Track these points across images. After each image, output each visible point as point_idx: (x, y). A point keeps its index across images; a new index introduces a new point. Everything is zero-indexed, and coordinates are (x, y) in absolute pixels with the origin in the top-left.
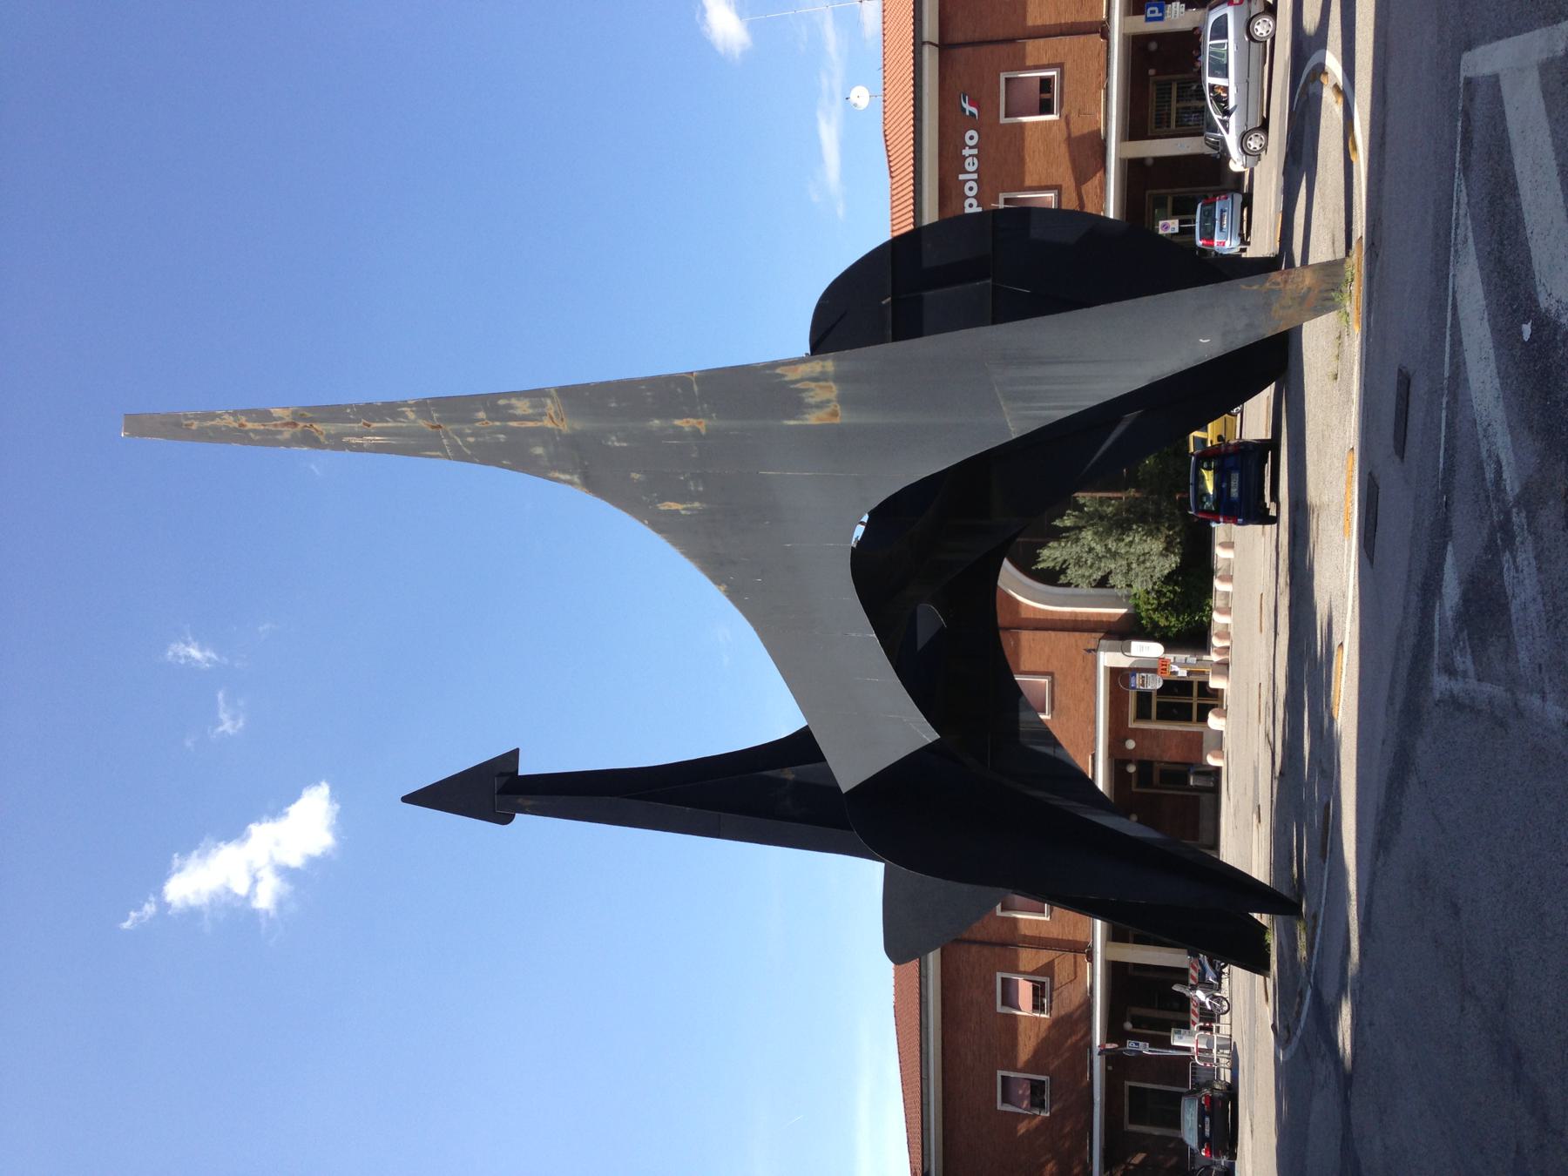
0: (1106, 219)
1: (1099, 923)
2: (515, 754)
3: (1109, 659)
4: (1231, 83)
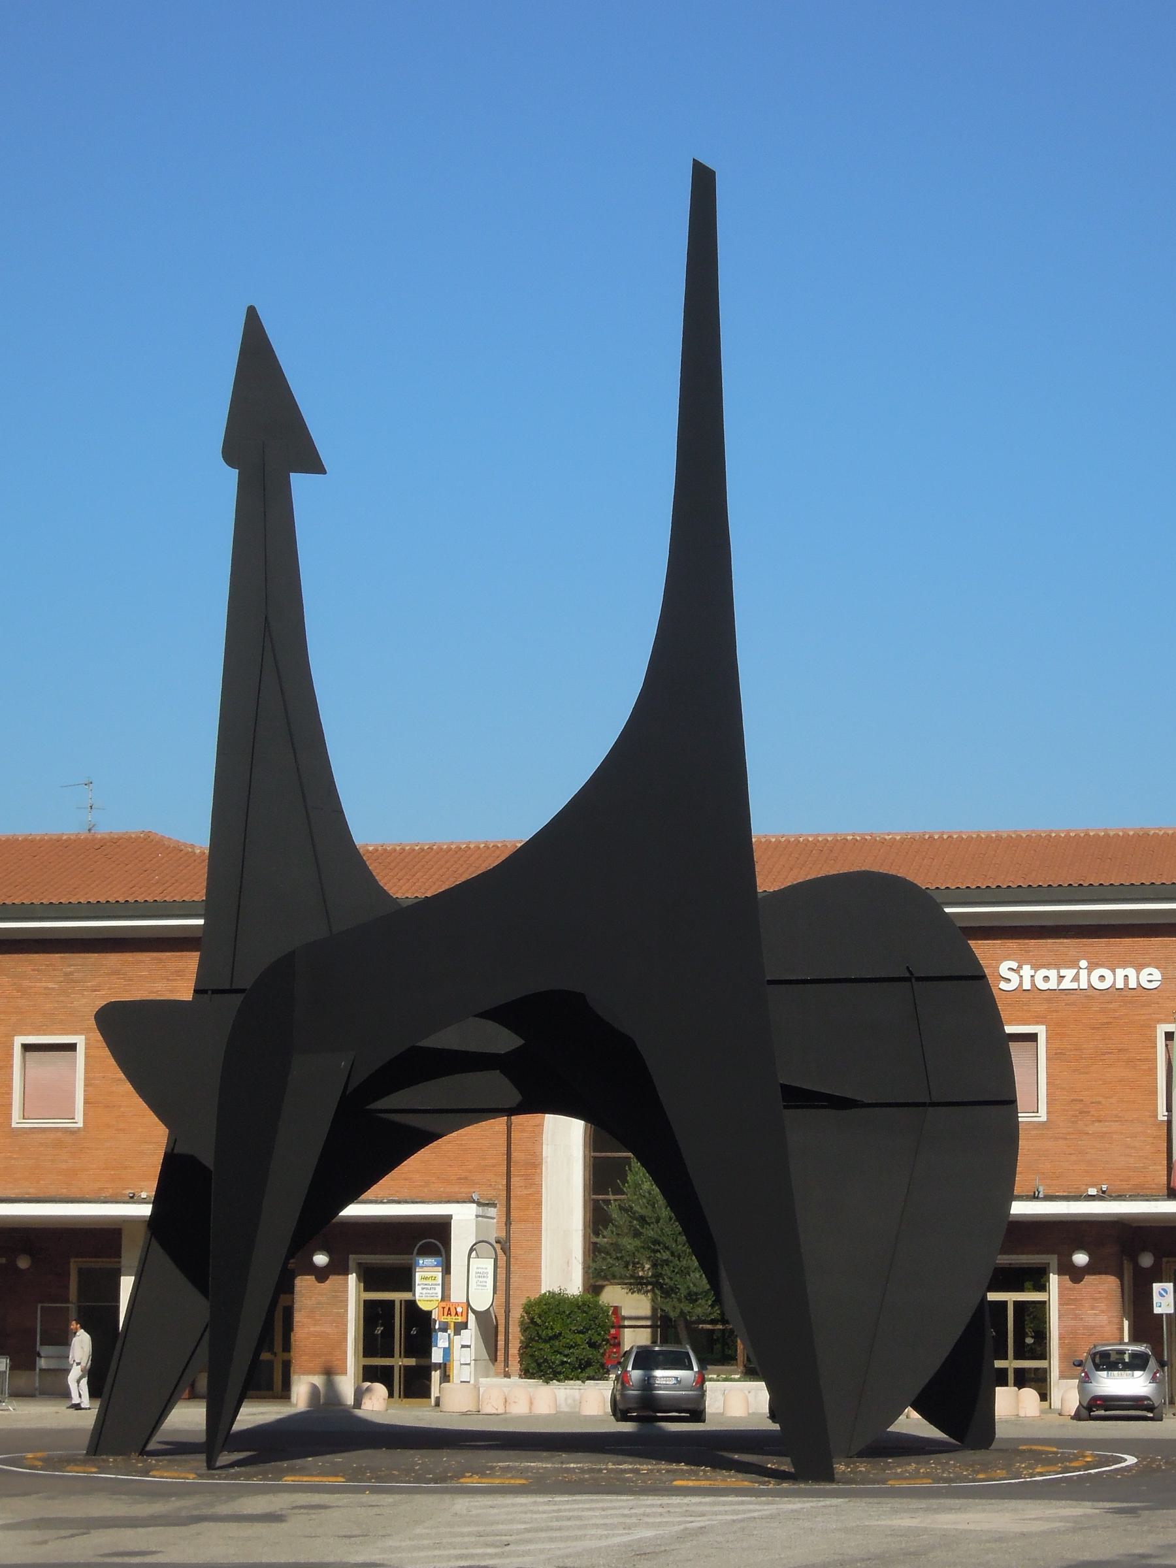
0: (1011, 1197)
1: (146, 1210)
2: (314, 465)
3: (465, 1220)
4: (771, 1486)
